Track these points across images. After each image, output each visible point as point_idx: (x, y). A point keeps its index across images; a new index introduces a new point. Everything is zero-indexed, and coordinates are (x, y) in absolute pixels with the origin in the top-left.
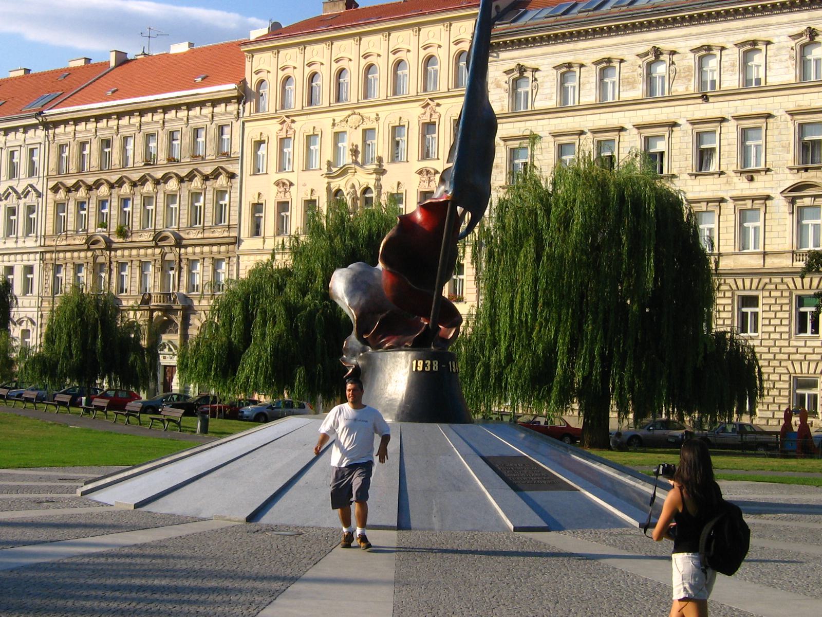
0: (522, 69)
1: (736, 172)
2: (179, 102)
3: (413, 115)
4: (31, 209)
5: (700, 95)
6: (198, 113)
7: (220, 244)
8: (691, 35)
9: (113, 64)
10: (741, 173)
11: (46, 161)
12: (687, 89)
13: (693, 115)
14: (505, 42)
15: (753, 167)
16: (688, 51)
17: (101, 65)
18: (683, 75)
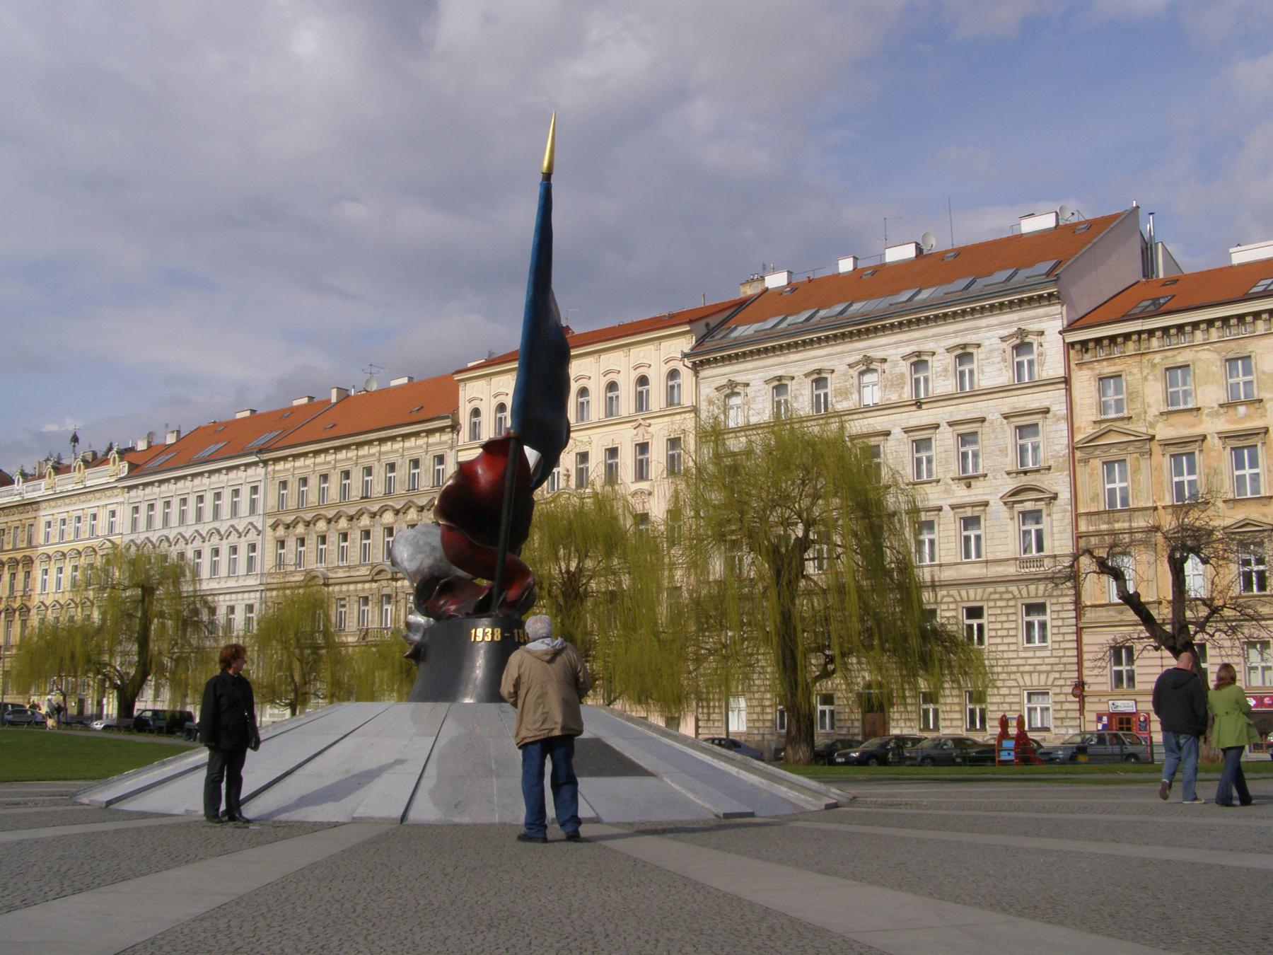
0: (732, 384)
1: (953, 479)
3: (625, 438)
4: (253, 547)
5: (914, 402)
7: (273, 589)
8: (939, 335)
9: (334, 400)
10: (959, 479)
11: (267, 499)
12: (900, 396)
13: (908, 422)
14: (715, 359)
15: (970, 472)
17: (323, 402)
18: (895, 383)
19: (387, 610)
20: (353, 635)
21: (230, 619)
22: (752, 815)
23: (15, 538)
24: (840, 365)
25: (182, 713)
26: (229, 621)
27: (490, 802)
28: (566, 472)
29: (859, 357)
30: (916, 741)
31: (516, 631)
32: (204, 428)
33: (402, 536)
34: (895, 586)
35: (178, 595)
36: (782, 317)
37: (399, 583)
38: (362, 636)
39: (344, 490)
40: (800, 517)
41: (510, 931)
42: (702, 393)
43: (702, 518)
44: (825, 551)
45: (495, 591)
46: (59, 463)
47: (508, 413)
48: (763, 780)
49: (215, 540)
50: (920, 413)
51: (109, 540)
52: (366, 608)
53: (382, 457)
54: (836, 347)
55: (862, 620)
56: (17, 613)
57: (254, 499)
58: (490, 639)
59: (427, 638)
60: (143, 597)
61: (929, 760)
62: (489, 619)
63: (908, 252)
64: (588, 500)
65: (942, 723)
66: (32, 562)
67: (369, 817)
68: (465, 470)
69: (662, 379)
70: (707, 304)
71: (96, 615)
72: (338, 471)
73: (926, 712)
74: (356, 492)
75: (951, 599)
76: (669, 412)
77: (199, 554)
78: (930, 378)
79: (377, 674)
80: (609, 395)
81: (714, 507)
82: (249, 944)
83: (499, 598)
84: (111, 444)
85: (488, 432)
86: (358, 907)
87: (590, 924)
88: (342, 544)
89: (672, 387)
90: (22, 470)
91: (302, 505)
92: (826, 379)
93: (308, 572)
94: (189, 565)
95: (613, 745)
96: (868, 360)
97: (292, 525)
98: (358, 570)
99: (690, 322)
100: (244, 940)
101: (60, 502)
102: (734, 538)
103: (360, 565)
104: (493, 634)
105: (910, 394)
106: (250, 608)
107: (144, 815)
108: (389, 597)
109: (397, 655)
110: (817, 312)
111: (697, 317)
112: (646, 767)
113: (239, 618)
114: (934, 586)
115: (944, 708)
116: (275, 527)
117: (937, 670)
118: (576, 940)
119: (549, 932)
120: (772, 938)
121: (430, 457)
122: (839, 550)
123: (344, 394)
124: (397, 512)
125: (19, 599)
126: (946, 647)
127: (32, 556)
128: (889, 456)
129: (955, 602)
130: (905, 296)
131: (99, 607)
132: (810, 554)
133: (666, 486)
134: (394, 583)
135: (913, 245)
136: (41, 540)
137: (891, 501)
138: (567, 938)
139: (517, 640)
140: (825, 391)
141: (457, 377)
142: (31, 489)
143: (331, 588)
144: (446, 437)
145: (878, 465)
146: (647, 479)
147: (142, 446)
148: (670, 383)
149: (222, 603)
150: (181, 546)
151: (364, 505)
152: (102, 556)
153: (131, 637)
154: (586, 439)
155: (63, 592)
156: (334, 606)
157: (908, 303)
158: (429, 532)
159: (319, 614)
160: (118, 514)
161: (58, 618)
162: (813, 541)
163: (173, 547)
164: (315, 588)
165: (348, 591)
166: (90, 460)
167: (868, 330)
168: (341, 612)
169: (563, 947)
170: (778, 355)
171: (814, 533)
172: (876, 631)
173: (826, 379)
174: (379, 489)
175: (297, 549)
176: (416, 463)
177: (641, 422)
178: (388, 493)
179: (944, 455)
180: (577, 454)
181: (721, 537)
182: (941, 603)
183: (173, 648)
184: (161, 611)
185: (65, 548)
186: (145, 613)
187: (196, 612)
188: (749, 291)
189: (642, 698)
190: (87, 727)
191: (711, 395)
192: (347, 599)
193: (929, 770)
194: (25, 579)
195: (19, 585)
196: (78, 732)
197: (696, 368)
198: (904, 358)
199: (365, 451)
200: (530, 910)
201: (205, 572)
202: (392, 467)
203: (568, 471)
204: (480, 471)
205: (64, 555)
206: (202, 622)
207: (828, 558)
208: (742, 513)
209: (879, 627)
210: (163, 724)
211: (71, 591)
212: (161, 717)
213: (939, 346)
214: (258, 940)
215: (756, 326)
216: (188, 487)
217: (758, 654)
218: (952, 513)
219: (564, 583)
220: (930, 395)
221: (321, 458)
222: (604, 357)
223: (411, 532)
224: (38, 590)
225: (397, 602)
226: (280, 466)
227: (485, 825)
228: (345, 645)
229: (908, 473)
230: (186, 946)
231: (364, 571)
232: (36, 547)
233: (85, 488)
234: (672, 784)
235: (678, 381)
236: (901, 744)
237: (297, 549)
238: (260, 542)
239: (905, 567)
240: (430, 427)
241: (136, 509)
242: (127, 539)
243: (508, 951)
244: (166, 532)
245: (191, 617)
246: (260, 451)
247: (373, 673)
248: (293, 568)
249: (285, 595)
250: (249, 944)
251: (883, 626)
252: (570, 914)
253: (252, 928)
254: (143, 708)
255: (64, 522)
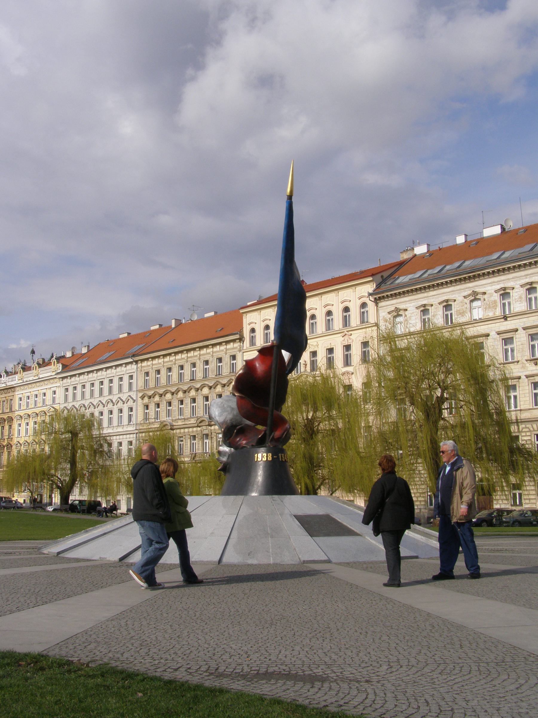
0: (397, 310)
1: (527, 361)
2: (207, 344)
4: (131, 409)
6: (218, 349)
7: (142, 432)
8: (494, 282)
9: (173, 326)
10: (531, 360)
11: (139, 382)
12: (494, 314)
13: (499, 328)
14: (387, 296)
16: (493, 292)
17: (167, 327)
19: (206, 443)
20: (188, 457)
21: (120, 449)
22: (417, 557)
23: (3, 407)
24: (459, 297)
25: (94, 501)
26: (119, 450)
27: (268, 552)
28: (304, 363)
29: (470, 292)
30: (509, 512)
31: (280, 455)
32: (102, 344)
33: (215, 403)
34: (494, 423)
35: (91, 437)
36: (424, 271)
37: (213, 428)
38: (193, 457)
39: (181, 376)
40: (439, 385)
41: (283, 627)
42: (380, 316)
43: (383, 387)
44: (453, 403)
45: (268, 432)
46: (25, 365)
47: (272, 331)
48: (422, 537)
49: (110, 405)
50: (506, 322)
51: (53, 407)
52: (194, 442)
53: (201, 357)
54: (456, 287)
55: (476, 443)
56: (6, 448)
57: (131, 382)
58: (265, 460)
59: (230, 460)
60: (72, 437)
61: (517, 523)
62: (265, 448)
63: (497, 230)
64: (318, 378)
65: (523, 501)
66: (13, 420)
67: (201, 561)
68: (249, 365)
69: (357, 308)
70: (382, 265)
71: (47, 448)
72: (177, 365)
73: (515, 495)
74: (187, 377)
75: (527, 430)
76: (361, 327)
77: (101, 413)
78: (512, 302)
79: (201, 478)
80: (328, 318)
81: (390, 380)
82: (138, 634)
83: (270, 436)
84: (53, 354)
85: (260, 343)
86: (197, 613)
87: (328, 623)
88: (180, 406)
89: (363, 313)
90: (6, 370)
91: (158, 385)
92: (451, 305)
93: (162, 423)
94: (96, 420)
95: (336, 518)
96: (475, 293)
97: (152, 396)
98: (190, 421)
99: (372, 275)
100: (135, 632)
101: (26, 387)
102: (401, 397)
103: (191, 418)
104: (267, 456)
105: (500, 312)
106: (130, 443)
107: (77, 560)
108: (207, 435)
109: (213, 468)
110: (445, 267)
111: (376, 272)
112: (355, 530)
113: (124, 449)
114: (517, 422)
115: (526, 493)
116: (143, 398)
117: (521, 471)
118: (320, 632)
119: (305, 627)
120: (433, 631)
121: (228, 356)
122: (462, 403)
123: (179, 323)
124: (210, 388)
125: (6, 440)
126: (525, 457)
127: (12, 416)
128: (490, 348)
129: (530, 431)
130: (495, 256)
131: (49, 444)
132: (446, 405)
133: (363, 369)
134: (210, 427)
135: (500, 226)
136: (17, 408)
137: (491, 374)
138: (315, 631)
139: (281, 460)
140: (451, 312)
141: (242, 311)
142: (10, 380)
143: (174, 431)
144: (237, 345)
145: (483, 354)
146: (351, 365)
147: (69, 354)
148: (362, 310)
149: (115, 441)
150: (92, 409)
151: (192, 384)
152: (49, 416)
153: (66, 460)
154: (315, 344)
155: (29, 436)
156: (177, 441)
157: (498, 260)
158: (230, 400)
159: (169, 445)
160: (57, 393)
161: (27, 450)
162: (447, 399)
163: (87, 410)
164: (166, 431)
165: (184, 432)
166: (41, 363)
167: (474, 276)
168: (181, 444)
169: (313, 636)
170: (423, 293)
171: (447, 393)
172: (484, 449)
173: (451, 305)
174: (200, 375)
175: (155, 409)
176: (220, 360)
177: (346, 333)
178: (205, 377)
179: (521, 347)
180: (310, 352)
181: (394, 397)
182: (522, 432)
183: (89, 466)
184: (81, 446)
185: (30, 412)
186: (73, 447)
187: (101, 446)
188: (406, 256)
189: (350, 489)
190: (44, 510)
191: (385, 316)
192: (184, 437)
193: (518, 529)
194: (9, 429)
195: (6, 433)
196: (39, 512)
197: (377, 301)
198: (496, 292)
199: (191, 354)
200: (293, 614)
201: (105, 424)
202: (207, 362)
203: (305, 362)
204: (257, 365)
205: (29, 416)
206: (104, 451)
207: (456, 408)
208: (406, 383)
209: (486, 447)
210: (85, 508)
211: (34, 435)
212: (84, 504)
213: (516, 284)
214: (143, 632)
215: (410, 277)
216: (123, 371)
217: (417, 463)
218: (526, 380)
219: (305, 426)
220: (512, 312)
221: (167, 359)
222: (324, 296)
223: (219, 400)
224: (16, 435)
225: (211, 438)
226: (145, 364)
227: (266, 565)
228: (183, 463)
229: (501, 357)
230: (104, 635)
231: (193, 421)
232: (14, 412)
233: (39, 378)
234: (371, 540)
235: (366, 309)
236: (500, 514)
237: (155, 409)
238: (135, 407)
239: (501, 412)
240: (227, 340)
241: (67, 390)
242: (62, 406)
243: (282, 639)
244: (83, 402)
245: (99, 449)
246: (134, 356)
247: (199, 478)
248: (153, 420)
249: (149, 436)
250: (138, 634)
251: (488, 446)
252: (316, 617)
253: (140, 625)
254: (74, 499)
255: (28, 397)
